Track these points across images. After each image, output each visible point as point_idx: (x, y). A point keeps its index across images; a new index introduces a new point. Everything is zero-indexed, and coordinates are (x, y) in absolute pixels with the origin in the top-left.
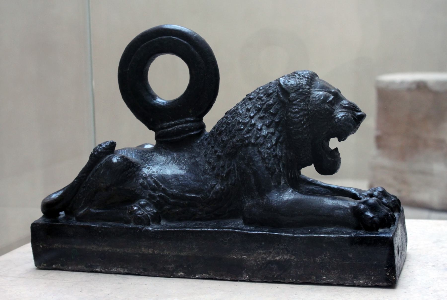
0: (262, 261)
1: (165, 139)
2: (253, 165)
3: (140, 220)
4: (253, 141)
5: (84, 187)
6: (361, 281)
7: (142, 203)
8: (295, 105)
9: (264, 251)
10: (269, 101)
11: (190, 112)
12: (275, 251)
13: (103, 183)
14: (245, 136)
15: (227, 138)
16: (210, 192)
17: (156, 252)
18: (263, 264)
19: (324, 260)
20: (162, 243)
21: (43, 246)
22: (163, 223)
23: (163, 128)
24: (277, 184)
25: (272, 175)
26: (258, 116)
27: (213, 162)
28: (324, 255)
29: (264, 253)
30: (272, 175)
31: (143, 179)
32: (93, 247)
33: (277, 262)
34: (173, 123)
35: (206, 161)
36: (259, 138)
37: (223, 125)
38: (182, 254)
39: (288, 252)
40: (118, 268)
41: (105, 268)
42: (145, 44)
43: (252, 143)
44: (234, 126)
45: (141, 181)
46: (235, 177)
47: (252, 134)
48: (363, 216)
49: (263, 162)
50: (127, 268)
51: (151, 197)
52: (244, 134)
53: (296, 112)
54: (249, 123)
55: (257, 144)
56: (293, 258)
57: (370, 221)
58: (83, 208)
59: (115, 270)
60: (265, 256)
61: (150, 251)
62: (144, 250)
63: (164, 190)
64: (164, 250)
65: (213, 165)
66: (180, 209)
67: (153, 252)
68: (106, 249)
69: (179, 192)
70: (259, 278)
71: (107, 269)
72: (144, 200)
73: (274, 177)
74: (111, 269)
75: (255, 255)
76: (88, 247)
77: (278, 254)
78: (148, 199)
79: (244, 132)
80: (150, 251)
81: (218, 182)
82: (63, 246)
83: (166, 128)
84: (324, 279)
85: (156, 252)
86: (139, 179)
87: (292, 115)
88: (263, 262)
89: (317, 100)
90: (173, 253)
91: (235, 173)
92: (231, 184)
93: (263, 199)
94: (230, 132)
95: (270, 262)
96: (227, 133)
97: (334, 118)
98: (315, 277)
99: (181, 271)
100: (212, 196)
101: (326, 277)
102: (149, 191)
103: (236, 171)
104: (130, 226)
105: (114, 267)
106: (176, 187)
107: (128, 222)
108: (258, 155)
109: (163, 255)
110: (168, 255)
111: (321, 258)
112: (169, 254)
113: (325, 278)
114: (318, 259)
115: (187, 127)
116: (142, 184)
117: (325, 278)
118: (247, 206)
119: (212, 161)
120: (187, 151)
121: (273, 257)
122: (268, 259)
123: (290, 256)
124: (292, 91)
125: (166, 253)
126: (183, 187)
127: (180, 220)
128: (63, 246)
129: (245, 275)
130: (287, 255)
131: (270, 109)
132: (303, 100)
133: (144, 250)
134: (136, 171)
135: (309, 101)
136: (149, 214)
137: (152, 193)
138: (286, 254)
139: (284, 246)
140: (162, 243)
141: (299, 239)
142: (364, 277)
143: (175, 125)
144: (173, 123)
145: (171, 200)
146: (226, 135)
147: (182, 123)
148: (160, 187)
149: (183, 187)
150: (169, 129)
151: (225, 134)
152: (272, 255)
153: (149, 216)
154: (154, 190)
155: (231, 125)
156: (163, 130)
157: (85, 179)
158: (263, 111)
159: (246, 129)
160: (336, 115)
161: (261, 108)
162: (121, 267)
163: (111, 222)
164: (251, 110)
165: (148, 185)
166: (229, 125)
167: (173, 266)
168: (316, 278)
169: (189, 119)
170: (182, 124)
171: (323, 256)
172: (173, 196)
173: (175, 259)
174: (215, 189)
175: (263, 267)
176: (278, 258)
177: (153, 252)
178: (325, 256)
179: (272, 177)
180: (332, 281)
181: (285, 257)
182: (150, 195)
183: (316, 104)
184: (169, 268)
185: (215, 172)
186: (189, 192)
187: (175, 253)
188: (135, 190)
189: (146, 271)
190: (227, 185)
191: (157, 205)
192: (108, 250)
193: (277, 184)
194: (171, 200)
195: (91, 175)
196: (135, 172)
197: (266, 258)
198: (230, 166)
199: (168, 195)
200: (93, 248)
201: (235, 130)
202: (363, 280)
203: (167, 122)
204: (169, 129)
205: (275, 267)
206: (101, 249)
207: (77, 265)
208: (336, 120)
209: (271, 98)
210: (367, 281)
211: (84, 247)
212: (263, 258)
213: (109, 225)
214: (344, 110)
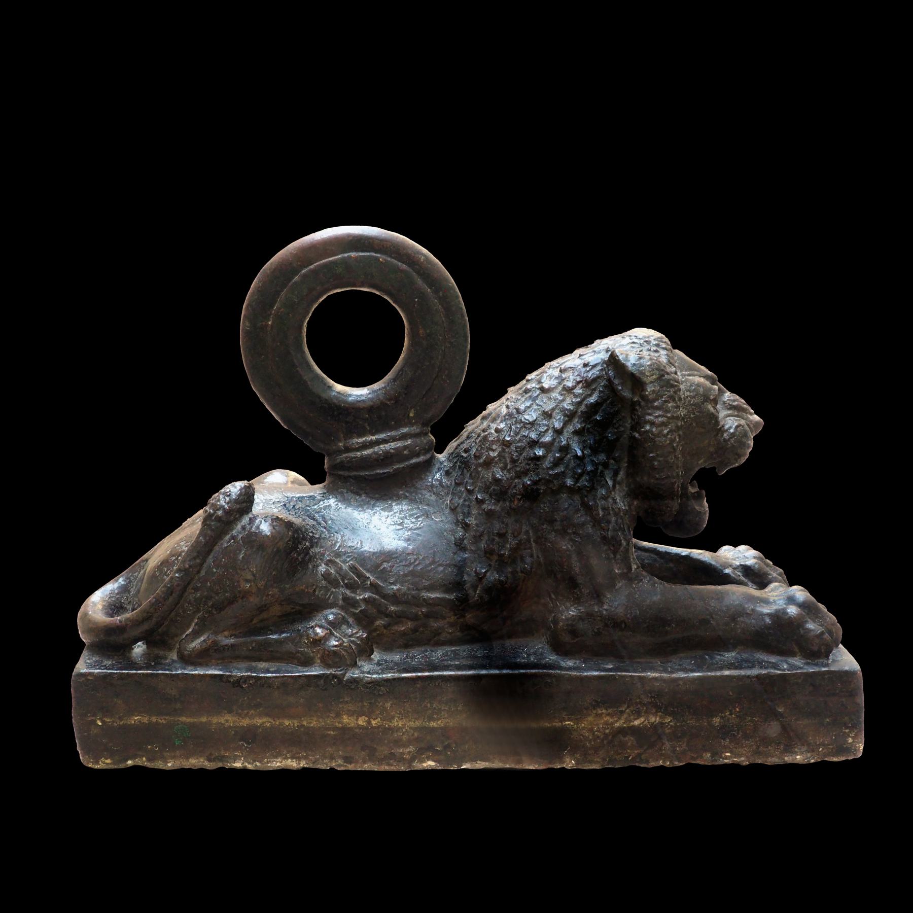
0: (605, 729)
1: (355, 473)
2: (574, 533)
3: (331, 658)
4: (569, 482)
5: (196, 589)
6: (798, 757)
7: (331, 617)
8: (657, 408)
9: (610, 711)
10: (590, 395)
11: (411, 415)
12: (632, 708)
13: (247, 581)
14: (551, 472)
15: (508, 476)
16: (475, 587)
17: (374, 723)
18: (606, 735)
19: (728, 719)
20: (388, 705)
21: (102, 721)
22: (376, 656)
23: (348, 449)
24: (625, 571)
25: (615, 553)
26: (571, 428)
27: (477, 525)
28: (731, 711)
29: (608, 715)
30: (615, 553)
31: (327, 564)
32: (228, 720)
33: (634, 731)
34: (373, 438)
35: (458, 521)
36: (581, 475)
37: (494, 447)
38: (433, 724)
39: (658, 708)
40: (287, 758)
41: (254, 761)
42: (312, 267)
43: (570, 487)
44: (521, 450)
45: (322, 568)
46: (532, 556)
47: (567, 467)
48: (802, 632)
49: (594, 526)
50: (305, 758)
51: (349, 603)
52: (548, 469)
53: (663, 424)
54: (556, 444)
55: (580, 489)
56: (668, 720)
57: (817, 641)
58: (196, 634)
59: (278, 764)
60: (611, 720)
61: (362, 721)
62: (346, 719)
63: (374, 587)
64: (393, 718)
65: (476, 531)
66: (410, 624)
67: (369, 722)
68: (258, 721)
69: (409, 589)
70: (598, 762)
71: (260, 762)
72: (334, 610)
73: (618, 556)
74: (268, 762)
75: (590, 719)
76: (215, 720)
77: (638, 715)
78: (342, 608)
79: (547, 464)
80: (362, 721)
81: (490, 565)
82: (154, 719)
83: (358, 450)
84: (726, 758)
85: (374, 723)
86: (318, 566)
87: (654, 430)
88: (607, 731)
90: (412, 724)
91: (531, 548)
92: (522, 572)
93: (601, 603)
94: (514, 461)
95: (622, 731)
96: (506, 465)
97: (720, 430)
98: (709, 755)
99: (428, 759)
100: (481, 597)
101: (731, 752)
102: (342, 589)
103: (534, 544)
104: (315, 671)
105: (276, 757)
106: (401, 579)
107: (307, 662)
108: (582, 512)
109: (390, 729)
110: (400, 728)
111: (722, 718)
112: (404, 725)
113: (728, 754)
114: (717, 721)
115: (405, 447)
116: (326, 576)
117: (728, 754)
118: (567, 619)
119: (471, 521)
120: (406, 497)
121: (628, 720)
122: (617, 725)
123: (661, 718)
124: (650, 379)
125: (397, 723)
126: (417, 579)
127: (406, 646)
128: (154, 719)
129: (568, 760)
130: (655, 714)
131: (596, 413)
132: (672, 398)
133: (346, 719)
134: (224, 509)
135: (680, 399)
136: (353, 642)
137: (348, 592)
138: (653, 714)
139: (652, 697)
140: (388, 705)
141: (681, 682)
142: (805, 748)
143: (378, 443)
144: (373, 438)
145: (393, 608)
146: (503, 469)
147: (394, 439)
148: (365, 581)
149: (417, 579)
150: (365, 452)
151: (501, 465)
152: (625, 716)
153: (354, 647)
154: (351, 586)
155: (513, 447)
156: (352, 455)
157: (199, 572)
158: (580, 417)
159: (550, 458)
160: (723, 426)
161: (576, 412)
162: (292, 758)
163: (266, 661)
164: (554, 414)
165: (339, 578)
166: (509, 447)
167: (412, 748)
168: (712, 757)
169: (405, 430)
170: (394, 440)
171: (727, 713)
172: (395, 598)
173: (416, 735)
174: (484, 581)
175: (605, 742)
176: (636, 723)
177: (369, 722)
178: (731, 714)
179: (615, 557)
180: (743, 759)
181: (652, 719)
182: (346, 599)
183: (692, 405)
184: (403, 753)
185: (482, 545)
186: (431, 588)
187: (418, 723)
188: (315, 591)
189: (351, 763)
190: (514, 573)
191: (364, 620)
192: (263, 723)
193: (625, 571)
194: (393, 608)
195: (210, 560)
196: (307, 550)
197: (612, 724)
198: (519, 534)
199: (384, 596)
200: (227, 721)
201: (525, 459)
202: (801, 754)
203: (360, 435)
204: (365, 452)
205: (630, 740)
206: (245, 722)
207: (187, 758)
208: (725, 435)
209: (595, 389)
210: (809, 755)
211: (204, 719)
212: (606, 723)
213: (268, 671)
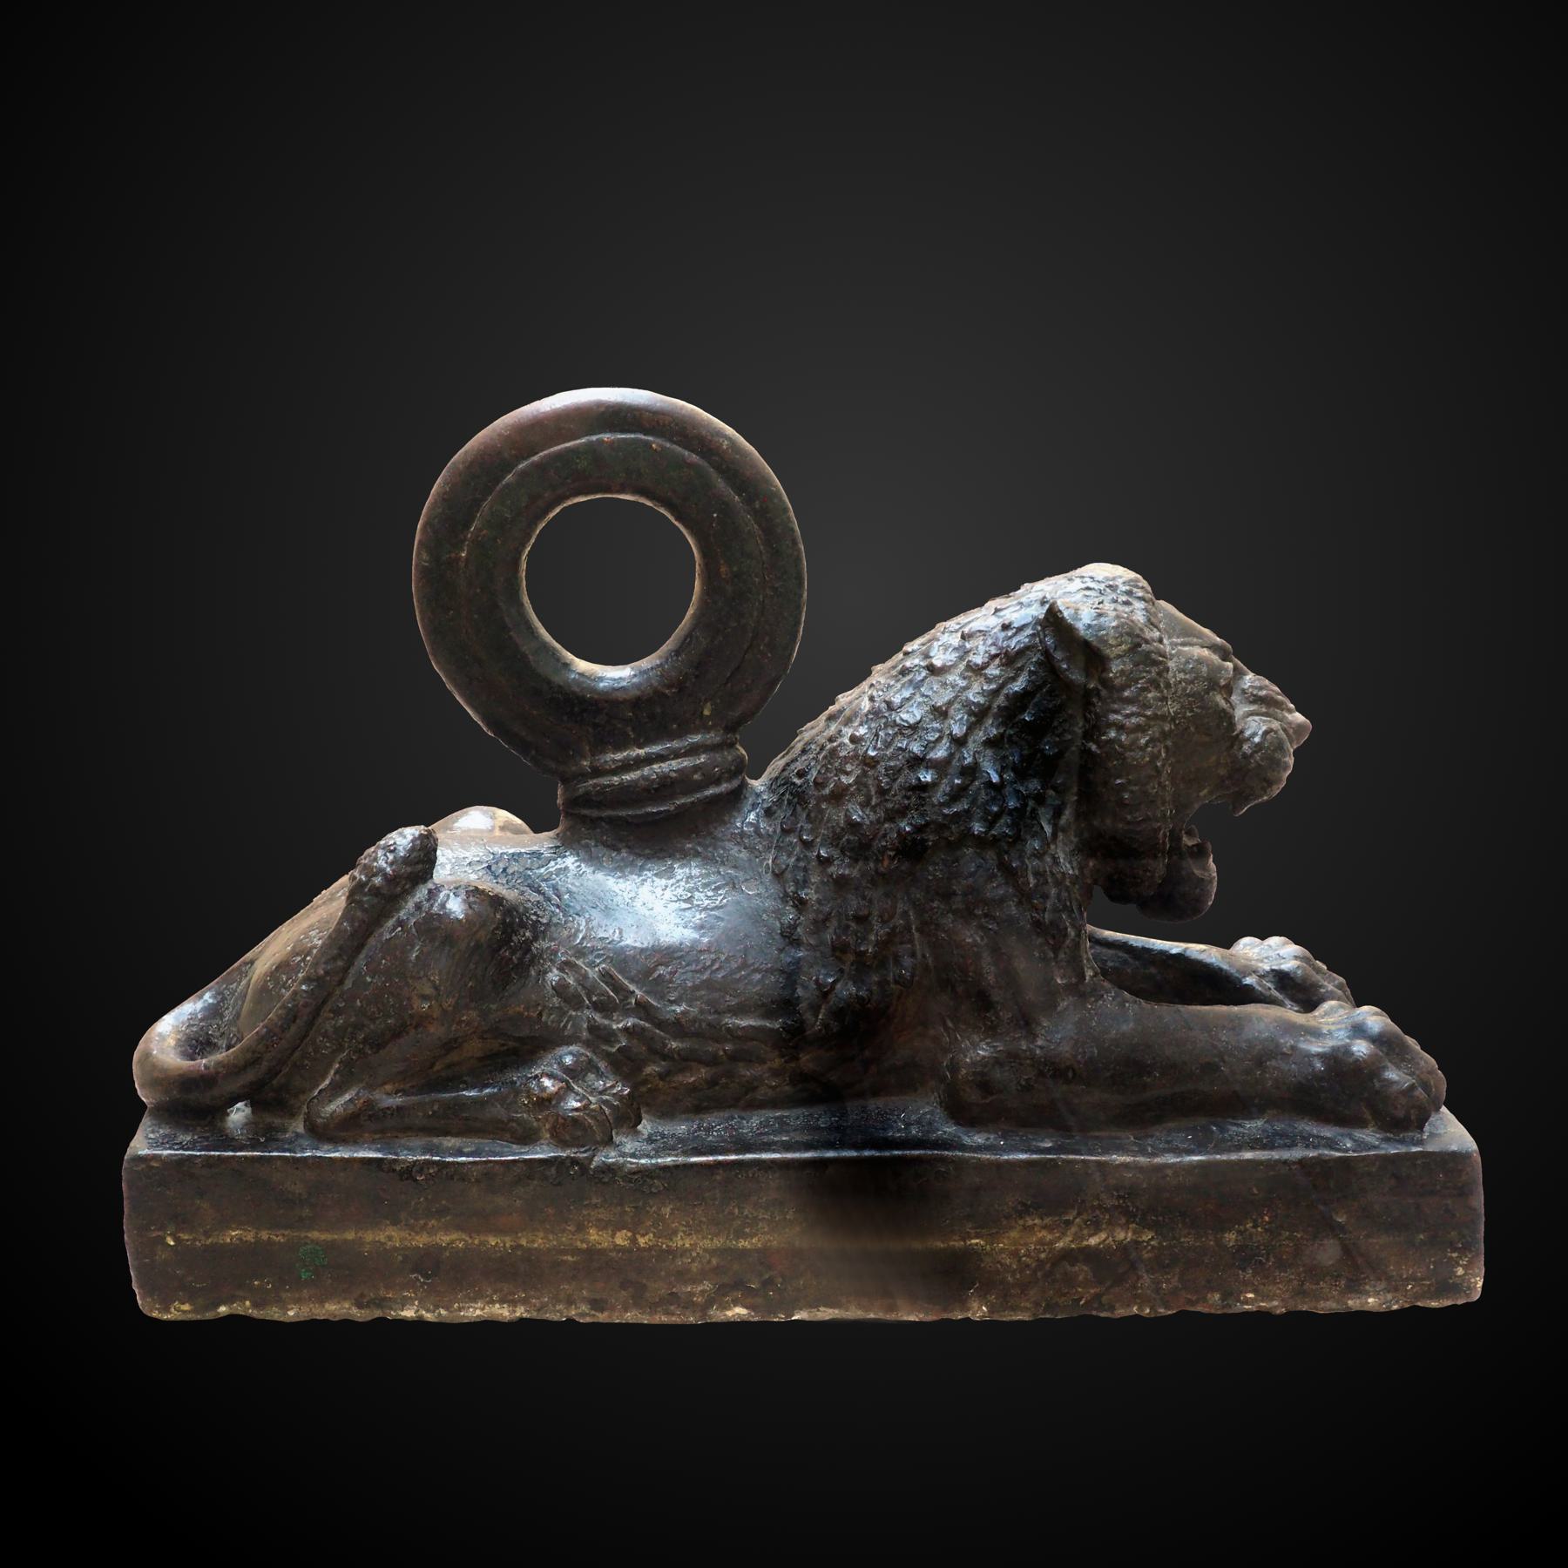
0: (1040, 1252)
1: (609, 813)
2: (986, 916)
3: (569, 1130)
4: (978, 828)
5: (337, 1012)
6: (1371, 1300)
7: (568, 1060)
8: (1129, 701)
9: (1047, 1221)
10: (1014, 679)
11: (706, 712)
12: (1085, 1217)
13: (424, 998)
14: (946, 811)
15: (873, 817)
16: (815, 1009)
17: (642, 1241)
18: (1041, 1263)
19: (1251, 1235)
20: (667, 1211)
21: (176, 1239)
22: (646, 1127)
23: (597, 772)
24: (1074, 980)
25: (1056, 949)
26: (980, 736)
27: (819, 901)
28: (1255, 1221)
29: (1045, 1227)
30: (1056, 949)
31: (561, 969)
32: (391, 1236)
33: (1089, 1255)
34: (641, 752)
35: (786, 895)
36: (997, 816)
37: (849, 768)
38: (743, 1243)
39: (1130, 1216)
40: (493, 1302)
41: (437, 1307)
42: (535, 458)
43: (978, 837)
44: (894, 773)
45: (554, 976)
46: (913, 955)
47: (973, 802)
48: (1377, 1085)
49: (1020, 903)
50: (525, 1301)
51: (599, 1036)
52: (942, 805)
53: (1139, 729)
54: (955, 763)
55: (996, 840)
56: (1147, 1236)
57: (1403, 1101)
58: (337, 1089)
59: (478, 1312)
60: (1049, 1237)
61: (621, 1239)
62: (594, 1235)
63: (643, 1009)
64: (675, 1233)
65: (818, 912)
66: (704, 1072)
67: (634, 1240)
68: (444, 1239)
69: (702, 1012)
70: (1026, 1309)
71: (447, 1309)
72: (573, 1048)
73: (1062, 956)
74: (460, 1309)
75: (1014, 1234)
76: (369, 1237)
77: (1096, 1227)
78: (587, 1044)
79: (939, 796)
80: (621, 1239)
81: (842, 971)
82: (264, 1235)
83: (614, 772)
84: (1247, 1302)
85: (642, 1241)
86: (546, 972)
87: (1123, 738)
88: (1043, 1256)
89: (1192, 682)
90: (707, 1243)
91: (911, 941)
92: (896, 982)
94: (882, 792)
95: (1067, 1256)
96: (869, 798)
97: (1237, 739)
98: (1217, 1296)
99: (736, 1303)
100: (826, 1026)
101: (1255, 1291)
102: (587, 1012)
103: (917, 935)
104: (541, 1153)
105: (475, 1300)
106: (688, 995)
107: (527, 1137)
108: (1000, 879)
109: (669, 1251)
110: (686, 1250)
111: (1240, 1232)
112: (694, 1246)
113: (1251, 1295)
114: (1231, 1238)
116: (560, 989)
117: (1251, 1295)
118: (974, 1064)
119: (809, 894)
120: (697, 854)
121: (1078, 1237)
122: (1060, 1245)
123: (1134, 1232)
124: (1116, 651)
125: (681, 1241)
126: (716, 995)
127: (698, 1110)
128: (264, 1235)
129: (975, 1305)
130: (1125, 1227)
131: (1023, 709)
132: (1154, 684)
133: (594, 1235)
135: (1168, 686)
136: (606, 1102)
137: (597, 1017)
138: (1122, 1226)
139: (1119, 1197)
140: (667, 1211)
141: (1169, 1172)
142: (1383, 1285)
143: (649, 760)
144: (641, 752)
145: (674, 1045)
146: (863, 806)
147: (676, 755)
148: (626, 998)
149: (716, 995)
151: (861, 799)
152: (1074, 1229)
153: (607, 1111)
154: (604, 1007)
155: (881, 769)
156: (605, 781)
157: (341, 982)
158: (996, 717)
159: (944, 787)
160: (1242, 732)
161: (989, 708)
162: (502, 1301)
163: (456, 1135)
164: (951, 712)
165: (583, 993)
166: (873, 767)
167: (707, 1285)
168: (1223, 1299)
169: (696, 738)
170: (677, 756)
171: (1249, 1225)
172: (678, 1027)
173: (714, 1261)
174: (832, 997)
175: (1039, 1274)
176: (1093, 1241)
177: (634, 1240)
178: (1255, 1227)
179: (1056, 956)
180: (1275, 1303)
181: (1121, 1235)
182: (593, 1028)
183: (1189, 695)
184: (691, 1294)
185: (829, 936)
186: (739, 1010)
187: (718, 1243)
188: (540, 1014)
189: (602, 1311)
190: (882, 984)
191: (624, 1065)
192: (452, 1242)
193: (1074, 980)
194: (674, 1045)
195: (361, 962)
196: (527, 944)
197: (1051, 1243)
198: (892, 917)
199: (660, 1024)
200: (390, 1238)
201: (902, 788)
202: (1376, 1294)
203: (619, 748)
205: (1082, 1271)
206: (421, 1240)
207: (322, 1303)
208: (1245, 747)
209: (1021, 669)
210: (1389, 1296)
211: (350, 1236)
212: (1041, 1242)
213: (460, 1152)
214: (1253, 708)
